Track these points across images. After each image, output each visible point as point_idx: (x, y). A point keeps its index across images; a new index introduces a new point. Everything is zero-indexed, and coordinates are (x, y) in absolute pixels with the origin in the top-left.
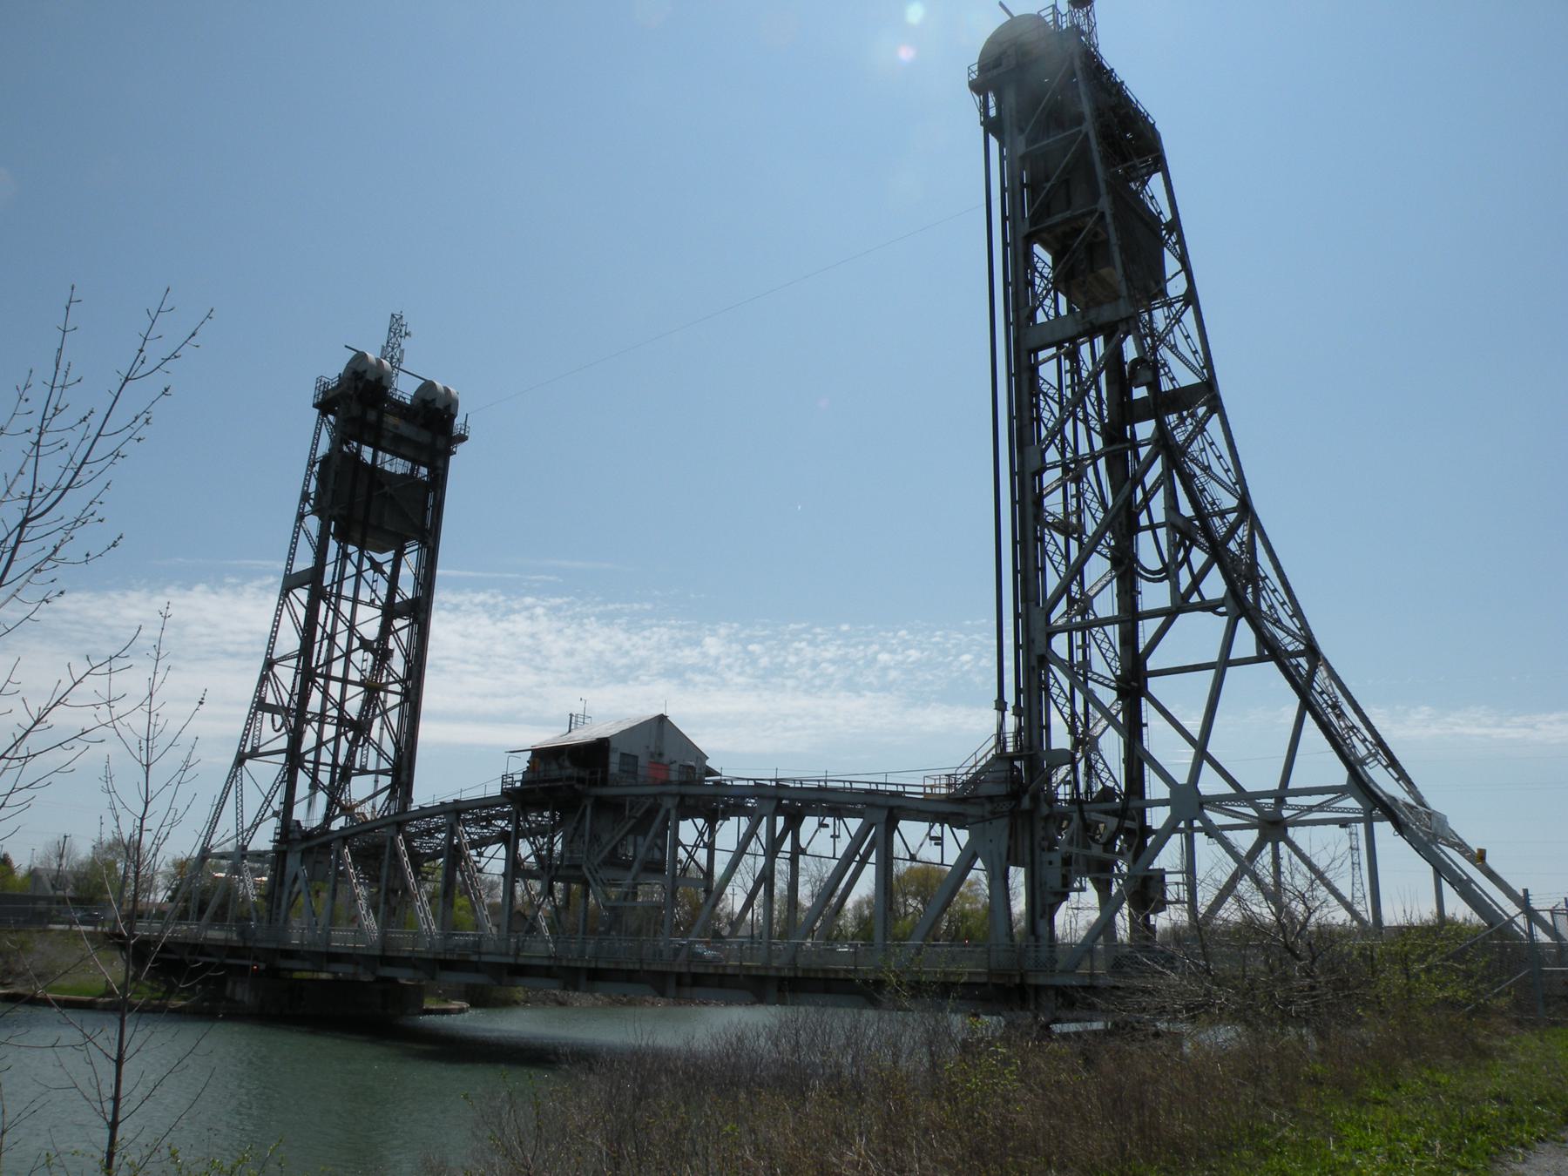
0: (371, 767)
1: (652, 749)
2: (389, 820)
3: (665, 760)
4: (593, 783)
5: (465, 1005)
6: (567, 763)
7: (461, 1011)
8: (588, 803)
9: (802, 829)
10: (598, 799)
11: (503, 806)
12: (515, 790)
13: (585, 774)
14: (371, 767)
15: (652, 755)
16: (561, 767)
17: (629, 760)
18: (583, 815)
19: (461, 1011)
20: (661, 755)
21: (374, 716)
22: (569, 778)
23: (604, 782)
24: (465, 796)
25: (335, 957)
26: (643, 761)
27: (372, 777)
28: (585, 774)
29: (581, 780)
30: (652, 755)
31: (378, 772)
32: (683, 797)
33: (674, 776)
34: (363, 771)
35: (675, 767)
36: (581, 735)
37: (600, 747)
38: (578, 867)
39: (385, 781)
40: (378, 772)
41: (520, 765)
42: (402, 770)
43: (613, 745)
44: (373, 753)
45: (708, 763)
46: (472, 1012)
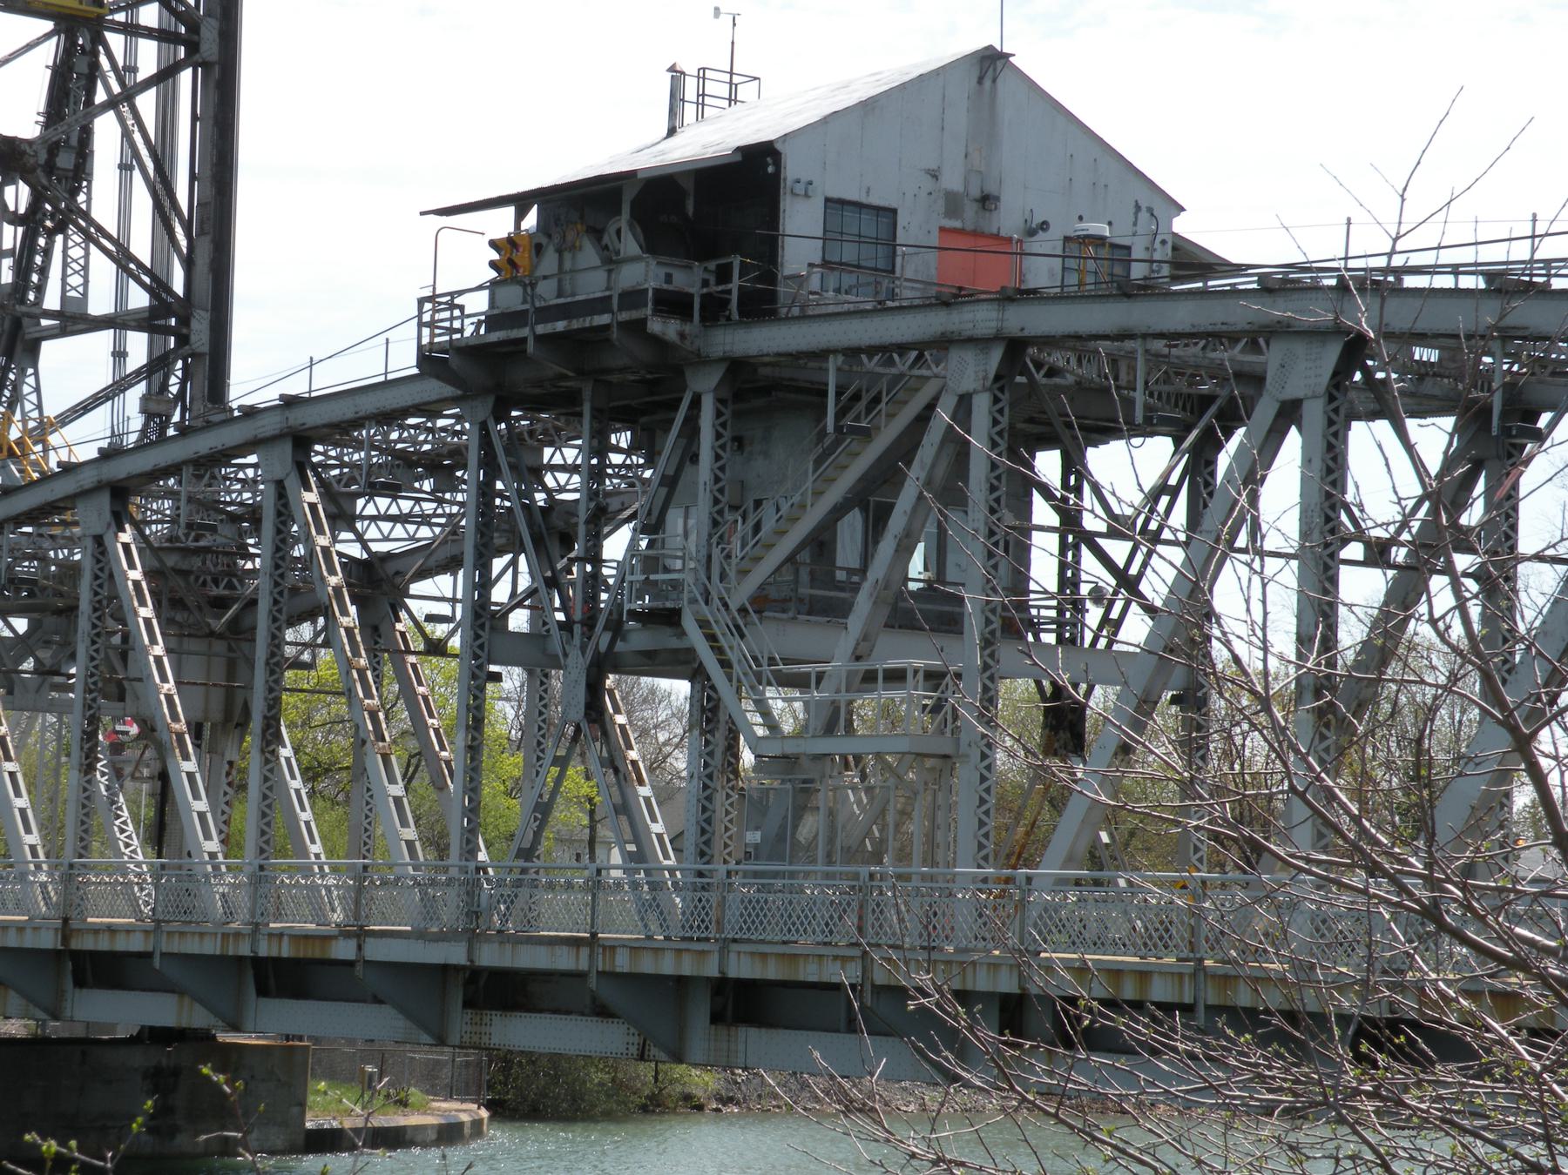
0: (100, 303)
1: (953, 181)
2: (87, 479)
3: (1008, 221)
4: (714, 310)
5: (466, 1111)
6: (630, 245)
7: (449, 1134)
8: (705, 384)
9: (1530, 478)
10: (738, 369)
11: (430, 410)
12: (471, 352)
13: (690, 280)
14: (100, 303)
15: (953, 204)
16: (611, 261)
17: (864, 225)
18: (691, 429)
19: (449, 1134)
20: (987, 201)
21: (94, 111)
22: (632, 298)
23: (761, 305)
24: (329, 379)
25: (106, 969)
26: (916, 226)
27: (106, 337)
28: (690, 280)
29: (672, 304)
30: (953, 204)
31: (118, 322)
32: (1016, 347)
33: (1042, 273)
34: (74, 320)
35: (1047, 243)
36: (710, 137)
37: (751, 176)
38: (669, 618)
39: (138, 347)
40: (118, 322)
41: (468, 264)
42: (189, 319)
43: (793, 169)
44: (103, 269)
45: (1182, 226)
46: (500, 1136)
